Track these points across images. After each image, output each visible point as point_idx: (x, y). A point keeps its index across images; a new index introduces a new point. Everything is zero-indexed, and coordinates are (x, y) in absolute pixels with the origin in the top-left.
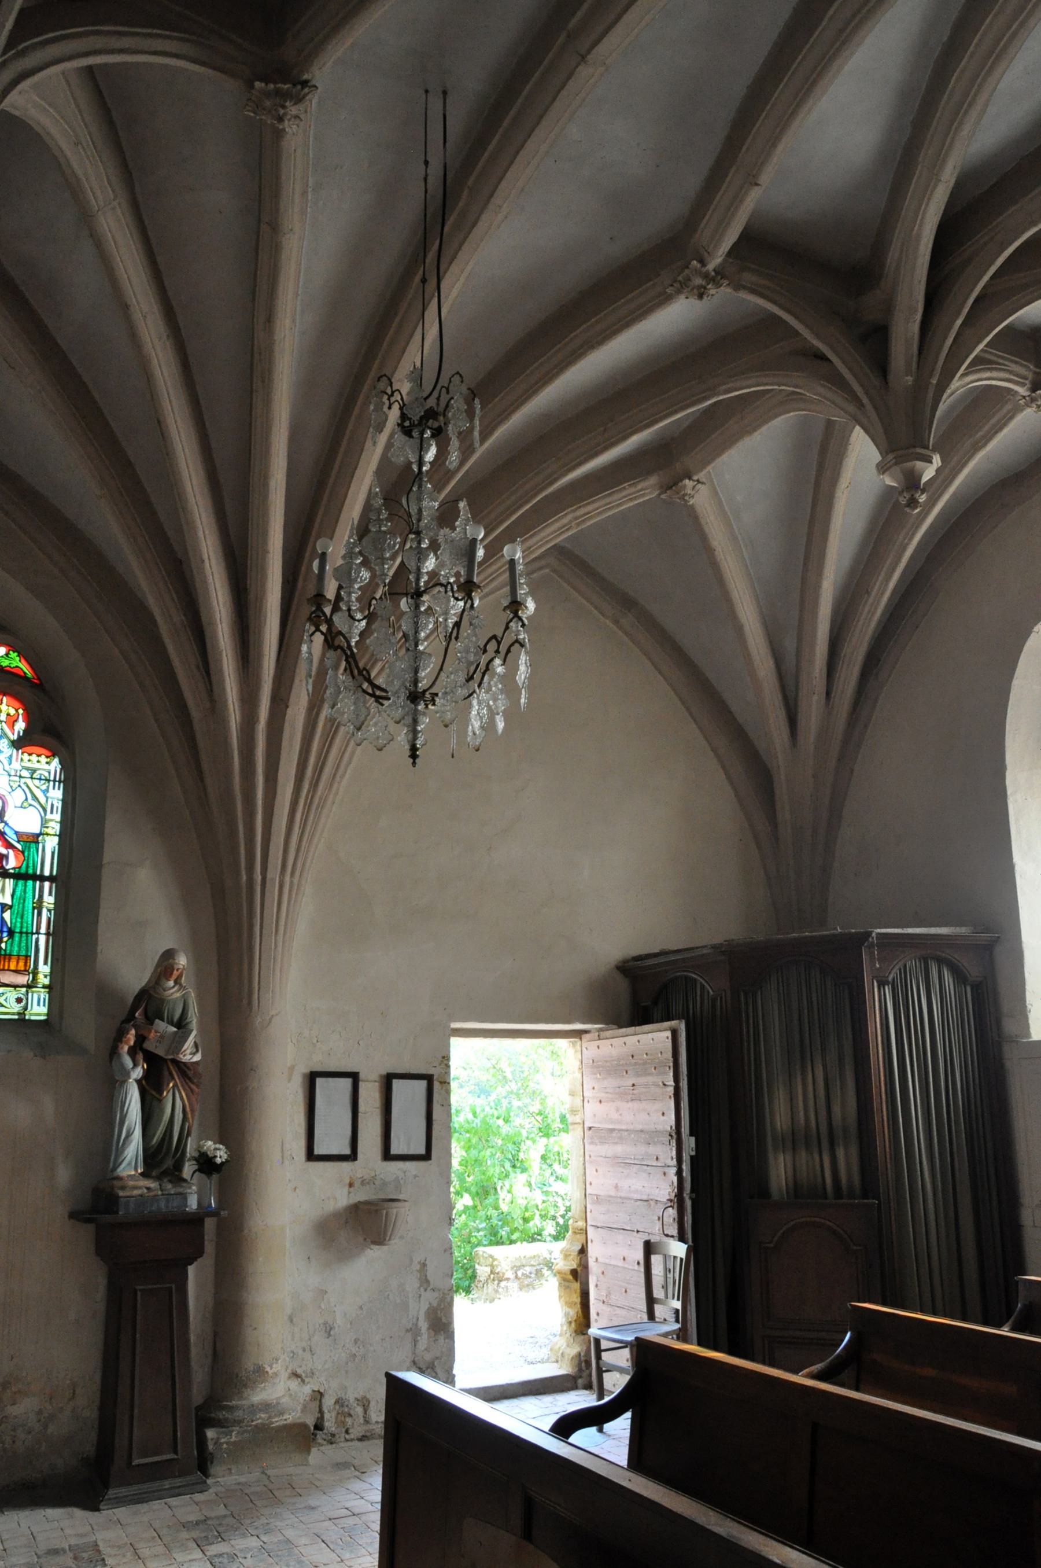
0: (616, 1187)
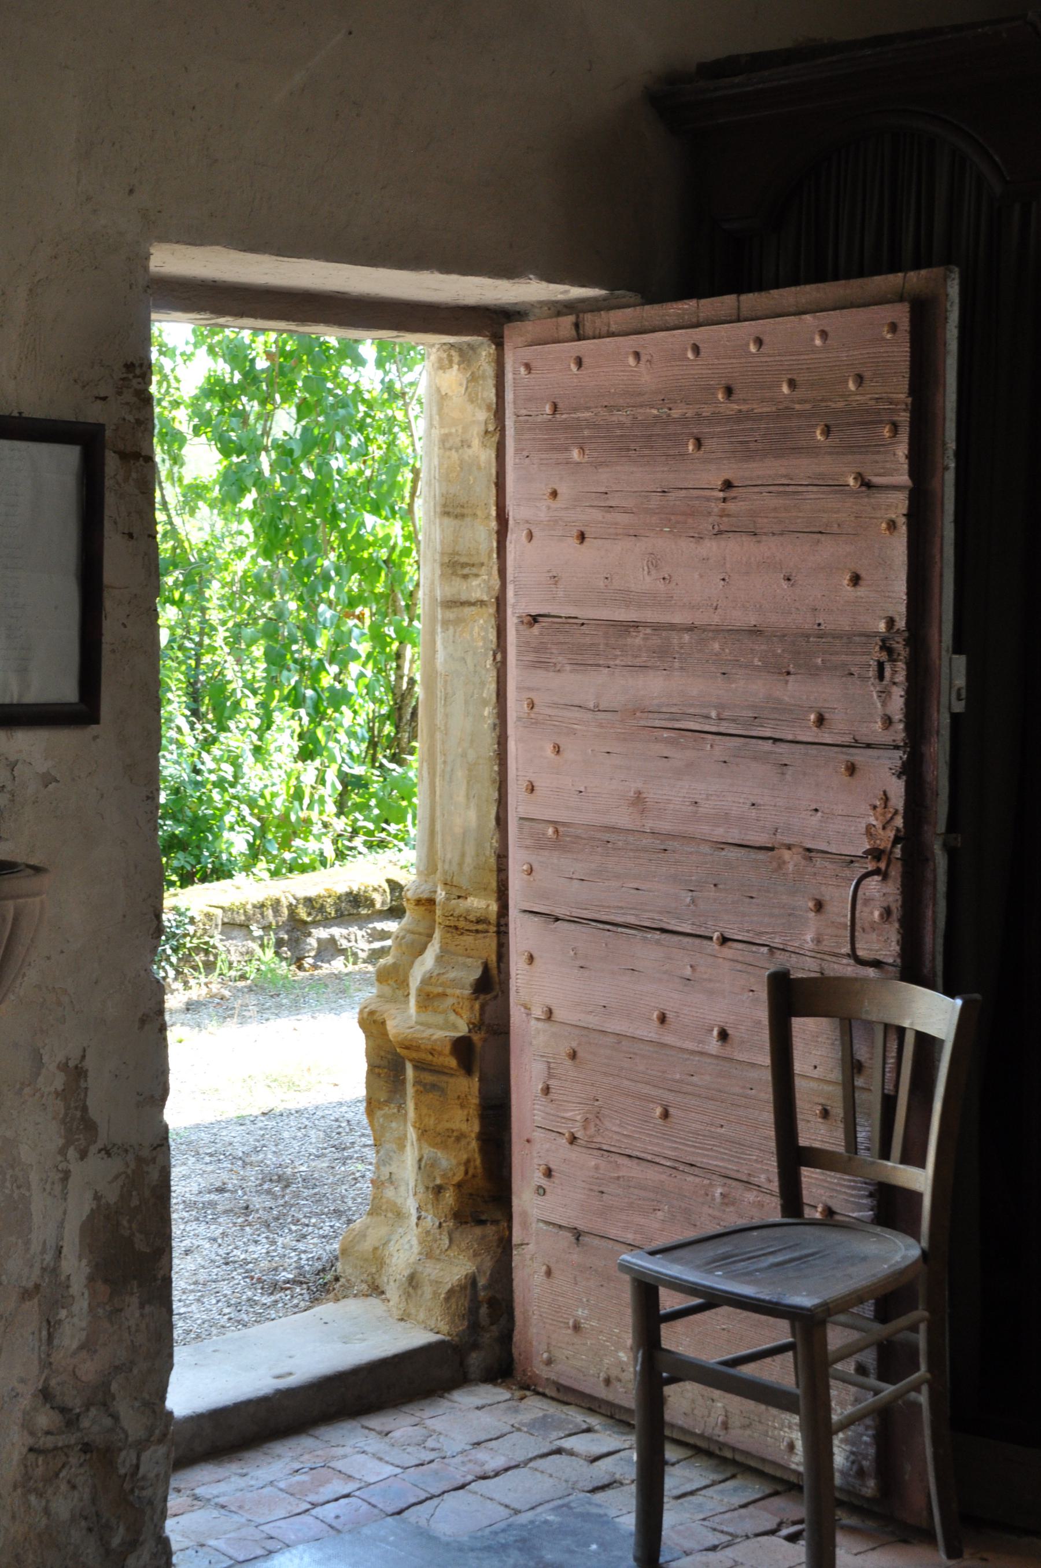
0: (638, 800)
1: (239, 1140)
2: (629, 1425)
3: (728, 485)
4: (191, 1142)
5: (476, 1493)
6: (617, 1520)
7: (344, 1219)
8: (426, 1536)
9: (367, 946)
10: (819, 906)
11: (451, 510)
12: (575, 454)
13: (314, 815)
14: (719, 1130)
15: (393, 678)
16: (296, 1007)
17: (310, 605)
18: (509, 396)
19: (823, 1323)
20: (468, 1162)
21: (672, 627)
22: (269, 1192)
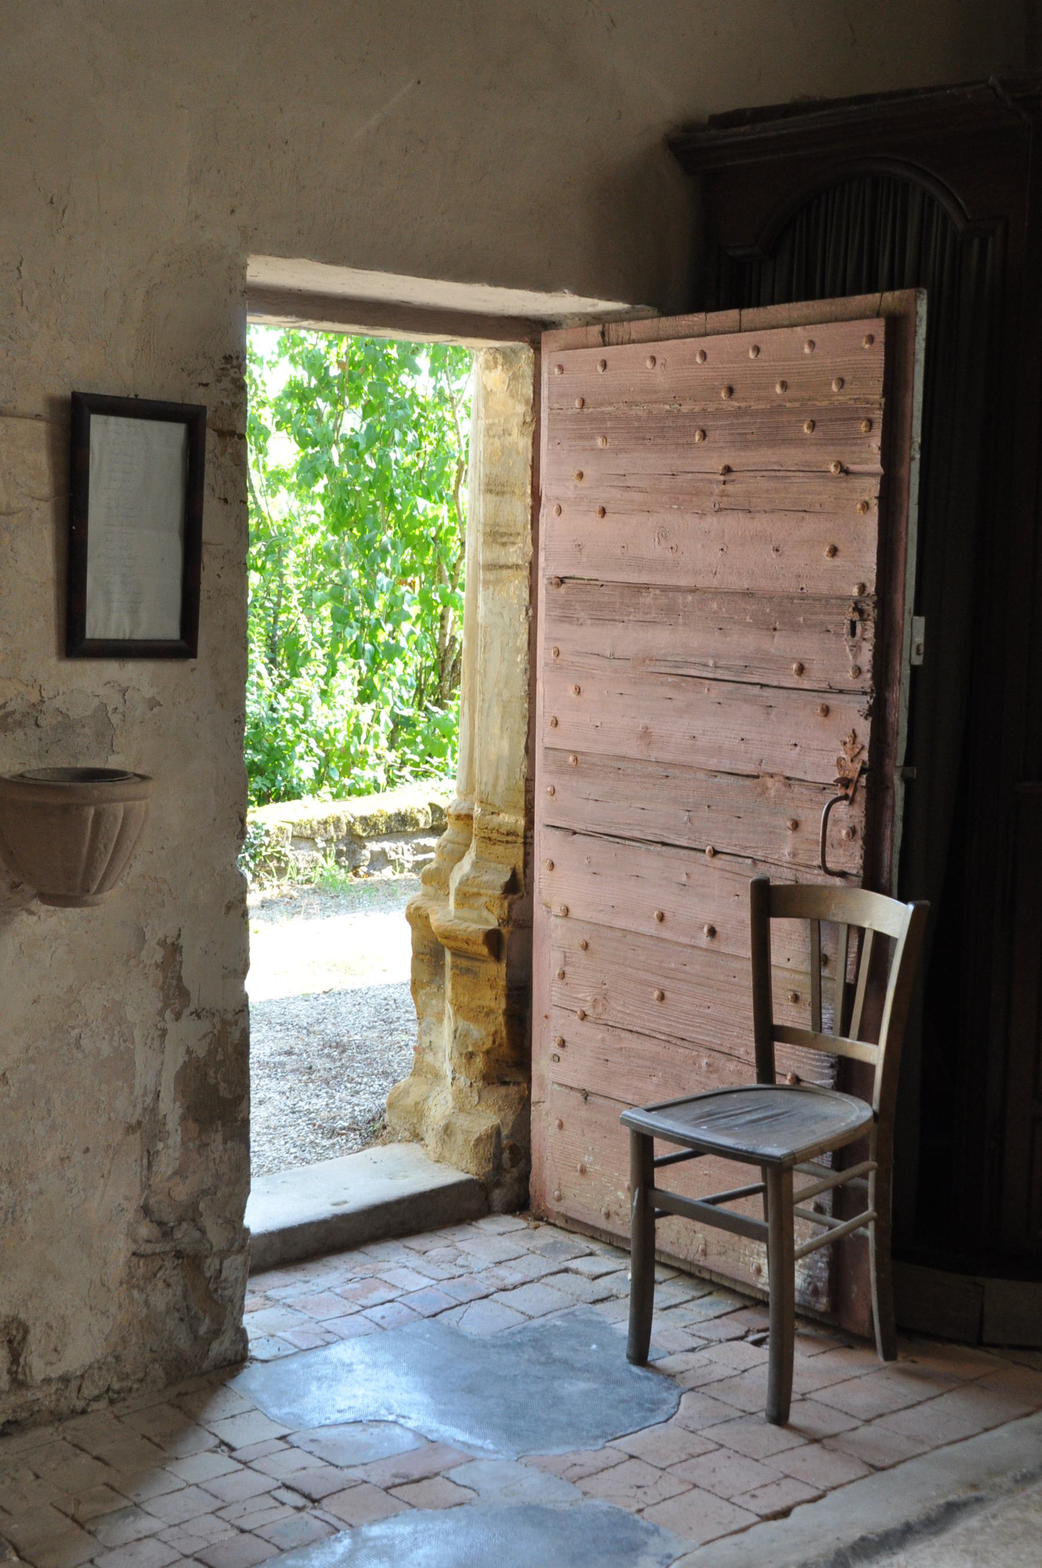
0: (646, 734)
1: (304, 1013)
2: (624, 1250)
3: (728, 470)
4: (265, 1014)
5: (497, 1302)
6: (613, 1326)
7: (390, 1079)
8: (456, 1335)
9: (412, 858)
10: (796, 825)
11: (493, 488)
12: (599, 442)
13: (370, 748)
14: (707, 1011)
15: (437, 636)
16: (352, 906)
17: (370, 574)
18: (544, 392)
19: (790, 1170)
20: (496, 1032)
21: (677, 589)
22: (328, 1056)
